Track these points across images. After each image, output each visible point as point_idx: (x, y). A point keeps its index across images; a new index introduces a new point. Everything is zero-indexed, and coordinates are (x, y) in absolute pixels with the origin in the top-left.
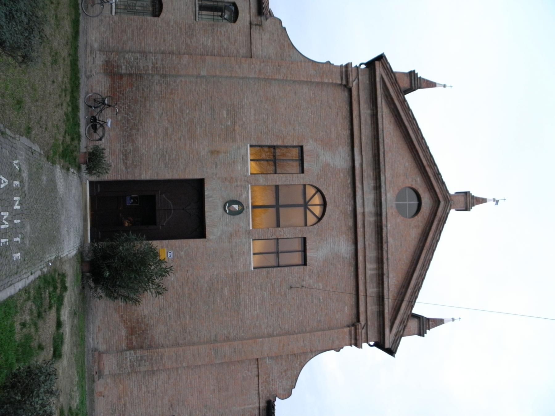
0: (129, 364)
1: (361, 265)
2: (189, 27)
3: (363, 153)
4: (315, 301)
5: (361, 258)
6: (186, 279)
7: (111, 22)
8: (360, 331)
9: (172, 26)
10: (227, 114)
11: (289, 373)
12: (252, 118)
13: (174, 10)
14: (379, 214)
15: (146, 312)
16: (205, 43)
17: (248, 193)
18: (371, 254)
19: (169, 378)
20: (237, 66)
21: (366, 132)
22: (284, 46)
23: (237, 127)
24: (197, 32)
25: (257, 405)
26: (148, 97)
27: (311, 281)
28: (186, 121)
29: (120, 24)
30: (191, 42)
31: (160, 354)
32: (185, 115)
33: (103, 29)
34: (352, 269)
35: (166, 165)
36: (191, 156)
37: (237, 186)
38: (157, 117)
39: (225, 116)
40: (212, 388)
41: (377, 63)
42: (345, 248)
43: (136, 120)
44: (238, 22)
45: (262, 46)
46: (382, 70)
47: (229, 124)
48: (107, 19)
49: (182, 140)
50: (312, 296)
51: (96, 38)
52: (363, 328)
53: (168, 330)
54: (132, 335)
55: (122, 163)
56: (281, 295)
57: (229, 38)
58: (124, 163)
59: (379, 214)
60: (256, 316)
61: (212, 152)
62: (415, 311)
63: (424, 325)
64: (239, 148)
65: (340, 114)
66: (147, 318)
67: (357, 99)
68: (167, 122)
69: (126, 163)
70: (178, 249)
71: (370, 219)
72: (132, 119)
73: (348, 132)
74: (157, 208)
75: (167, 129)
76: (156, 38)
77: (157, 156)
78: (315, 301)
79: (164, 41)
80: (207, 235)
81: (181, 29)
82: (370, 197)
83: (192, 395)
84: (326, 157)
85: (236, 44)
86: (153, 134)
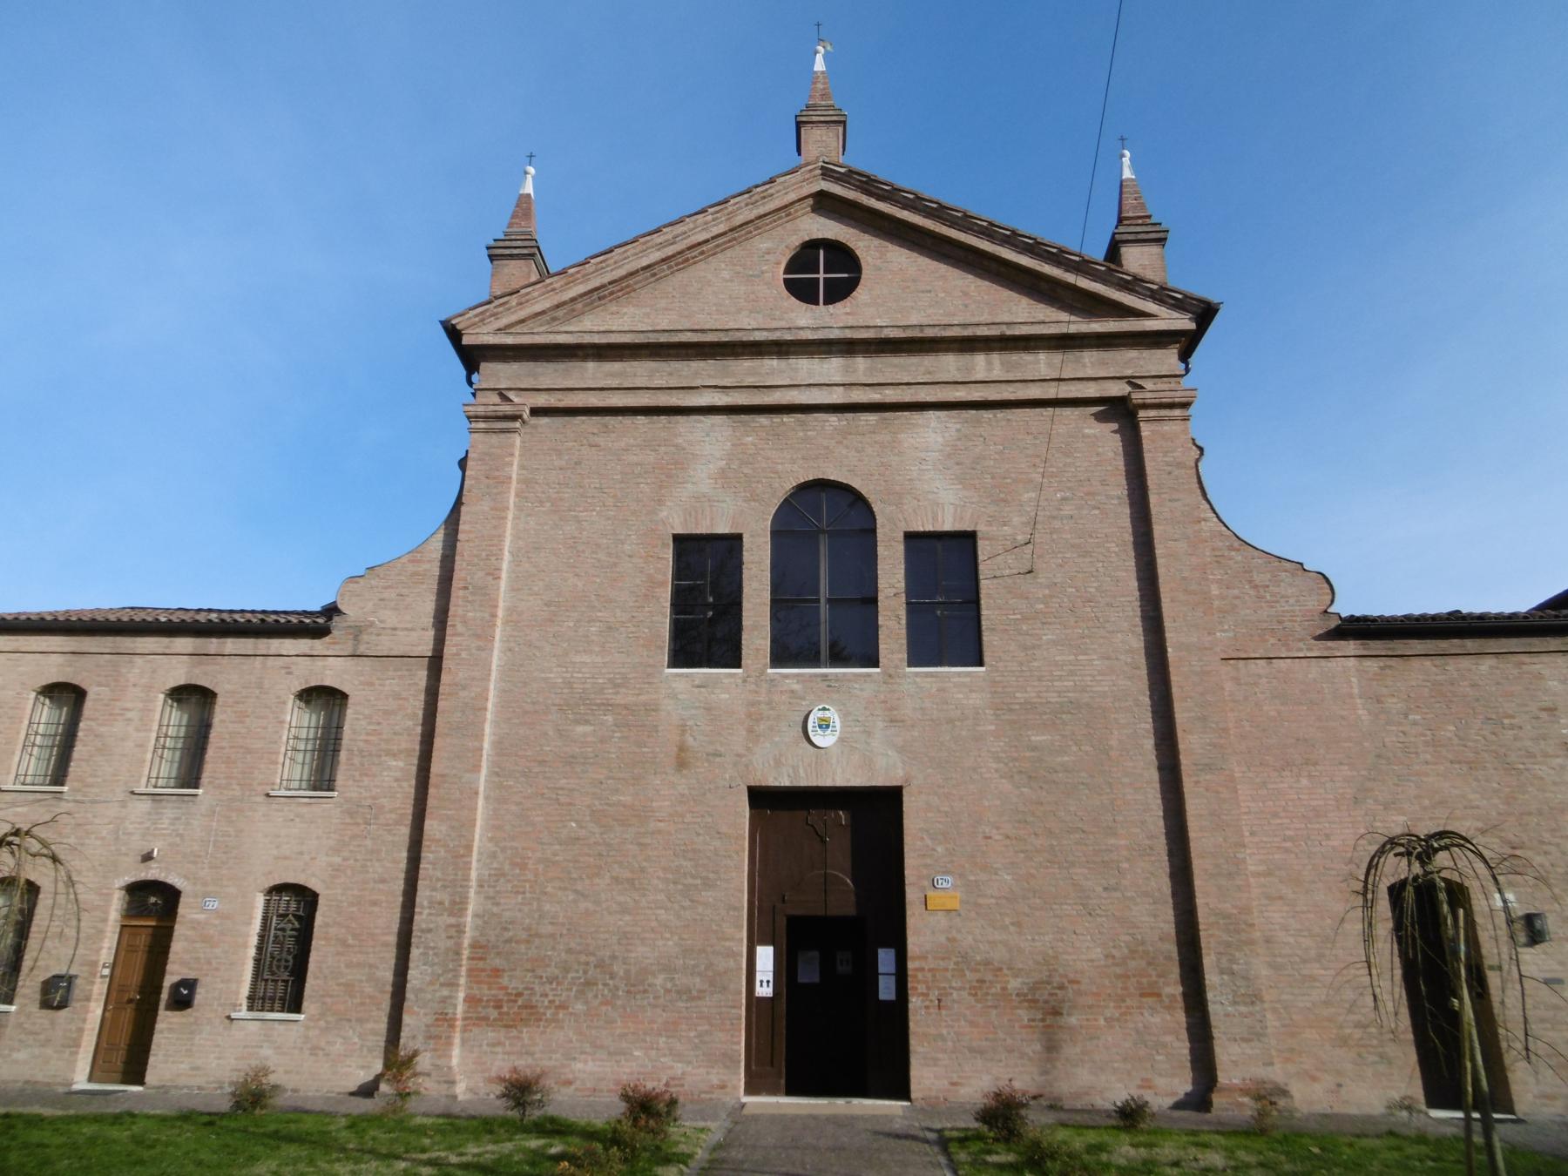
0: (1243, 1009)
1: (977, 394)
2: (351, 814)
3: (698, 383)
4: (1067, 510)
5: (960, 394)
6: (1008, 842)
7: (322, 1023)
8: (1149, 395)
9: (345, 859)
10: (587, 722)
11: (1258, 578)
12: (599, 659)
13: (301, 853)
14: (848, 347)
15: (1097, 953)
16: (398, 774)
17: (786, 676)
18: (949, 365)
19: (1281, 898)
20: (463, 694)
21: (640, 372)
22: (415, 574)
23: (619, 700)
24: (365, 794)
25: (1352, 662)
26: (529, 929)
27: (1016, 520)
28: (597, 830)
29: (329, 1000)
30: (391, 812)
31: (1213, 919)
32: (582, 833)
33: (338, 1047)
34: (987, 415)
35: (708, 884)
36: (688, 818)
37: (768, 704)
38: (583, 905)
39: (588, 728)
40: (1304, 782)
41: (466, 341)
42: (933, 431)
43: (587, 964)
44: (345, 689)
45: (412, 629)
46: (485, 329)
47: (610, 718)
48: (311, 1033)
49: (648, 841)
50: (1054, 518)
51: (363, 1067)
52: (1142, 387)
53: (1146, 894)
54: (1159, 995)
55: (700, 1003)
56: (1051, 596)
57: (386, 713)
58: (699, 998)
59: (848, 347)
60: (1107, 662)
61: (682, 764)
62: (1097, 252)
63: (501, 1080)
64: (674, 696)
65: (597, 440)
66: (1114, 952)
67: (559, 395)
68: (597, 880)
69: (700, 991)
70: (929, 861)
71: (861, 366)
72: (585, 972)
73: (641, 420)
74: (821, 913)
75: (616, 880)
76: (375, 903)
77: (684, 908)
78: (1067, 510)
79: (383, 881)
80: (895, 783)
81: (353, 837)
82: (806, 368)
83: (1328, 837)
84: (702, 477)
85: (404, 694)
86: (627, 918)
